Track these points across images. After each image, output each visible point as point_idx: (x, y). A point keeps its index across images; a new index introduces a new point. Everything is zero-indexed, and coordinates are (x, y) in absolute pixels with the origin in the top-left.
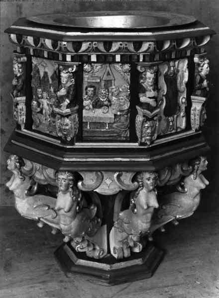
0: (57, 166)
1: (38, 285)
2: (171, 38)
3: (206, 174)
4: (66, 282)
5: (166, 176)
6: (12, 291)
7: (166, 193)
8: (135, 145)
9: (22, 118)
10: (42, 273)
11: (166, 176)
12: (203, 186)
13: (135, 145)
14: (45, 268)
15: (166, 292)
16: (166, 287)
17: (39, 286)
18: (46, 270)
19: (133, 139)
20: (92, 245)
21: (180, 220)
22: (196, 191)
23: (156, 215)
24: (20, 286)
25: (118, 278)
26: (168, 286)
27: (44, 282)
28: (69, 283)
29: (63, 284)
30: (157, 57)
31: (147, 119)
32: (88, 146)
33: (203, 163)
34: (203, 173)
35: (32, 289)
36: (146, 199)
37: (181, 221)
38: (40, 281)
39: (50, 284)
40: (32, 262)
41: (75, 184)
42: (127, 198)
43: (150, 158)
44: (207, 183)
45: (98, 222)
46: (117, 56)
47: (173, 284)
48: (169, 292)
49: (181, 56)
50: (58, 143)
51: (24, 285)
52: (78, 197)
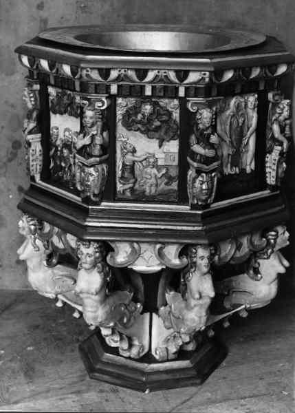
0: (81, 232)
1: (70, 396)
2: (262, 64)
3: (285, 252)
4: (107, 391)
5: (228, 250)
6: (35, 404)
7: (222, 274)
8: (184, 208)
9: (36, 166)
10: (75, 380)
11: (228, 250)
12: (282, 270)
13: (184, 208)
14: (79, 374)
15: (242, 405)
16: (242, 399)
17: (72, 398)
18: (81, 376)
19: (182, 197)
20: (126, 339)
21: (251, 310)
22: (274, 276)
23: (215, 306)
24: (46, 398)
25: (170, 381)
26: (245, 398)
27: (78, 392)
28: (111, 394)
29: (104, 394)
30: (214, 92)
31: (199, 172)
32: (126, 207)
33: (282, 237)
34: (281, 250)
35: (62, 402)
36: (202, 285)
37: (251, 312)
38: (74, 390)
39: (86, 395)
40: (62, 366)
41: (104, 259)
42: (175, 279)
43: (203, 226)
44: (286, 263)
45: (136, 308)
46: (260, 82)
47: (251, 395)
48: (245, 405)
51: (52, 397)
52: (108, 276)
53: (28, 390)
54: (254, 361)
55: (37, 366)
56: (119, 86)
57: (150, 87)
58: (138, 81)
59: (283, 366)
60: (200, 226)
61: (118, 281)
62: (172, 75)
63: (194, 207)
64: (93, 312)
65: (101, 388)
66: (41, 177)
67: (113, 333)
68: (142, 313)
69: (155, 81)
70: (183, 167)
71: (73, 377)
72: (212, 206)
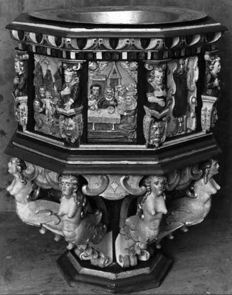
0: (61, 170)
3: (217, 178)
7: (175, 198)
8: (142, 147)
9: (24, 119)
10: (44, 282)
12: (214, 191)
13: (142, 147)
19: (141, 140)
20: (97, 253)
22: (207, 196)
23: (164, 222)
30: (166, 55)
31: (155, 119)
33: (214, 167)
34: (214, 177)
37: (190, 227)
38: (43, 290)
42: (133, 203)
44: (219, 187)
49: (191, 53)
50: (61, 145)
53: (7, 289)
54: (184, 268)
55: (14, 271)
56: (128, 53)
57: (126, 53)
58: (111, 49)
59: (207, 272)
60: (155, 161)
61: (91, 206)
62: (138, 44)
63: (149, 146)
64: (70, 230)
65: (64, 288)
66: (27, 127)
67: (87, 248)
68: (107, 232)
69: (93, 48)
70: (140, 114)
71: (43, 280)
72: (164, 144)
